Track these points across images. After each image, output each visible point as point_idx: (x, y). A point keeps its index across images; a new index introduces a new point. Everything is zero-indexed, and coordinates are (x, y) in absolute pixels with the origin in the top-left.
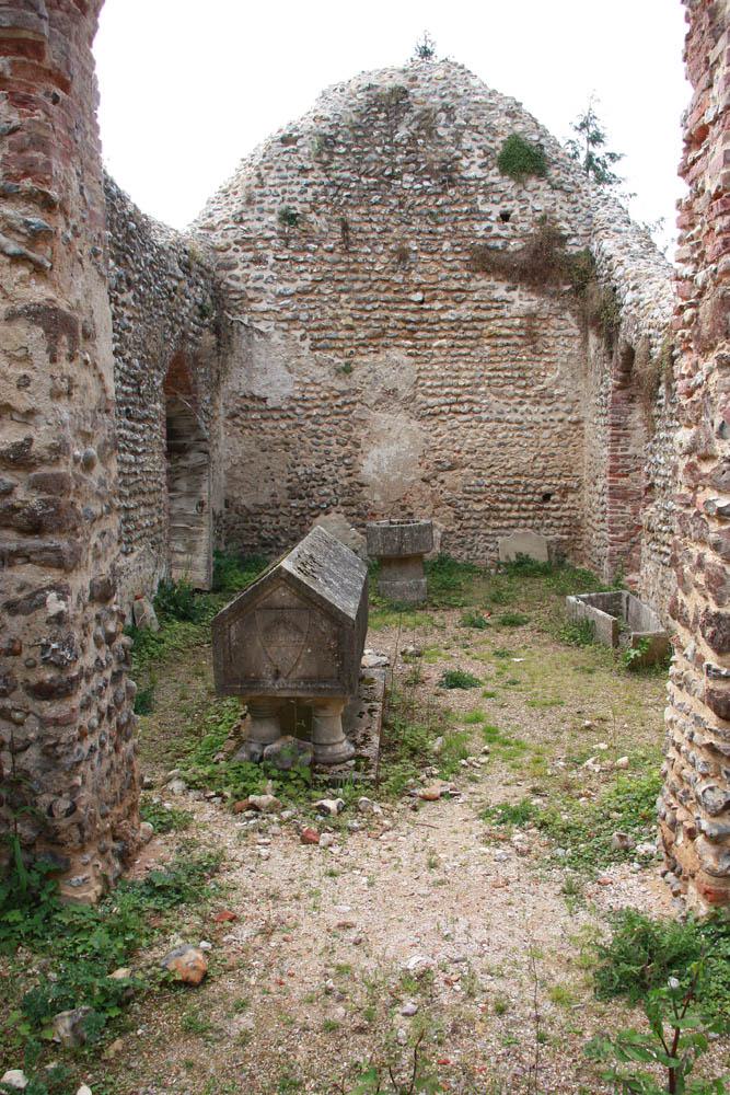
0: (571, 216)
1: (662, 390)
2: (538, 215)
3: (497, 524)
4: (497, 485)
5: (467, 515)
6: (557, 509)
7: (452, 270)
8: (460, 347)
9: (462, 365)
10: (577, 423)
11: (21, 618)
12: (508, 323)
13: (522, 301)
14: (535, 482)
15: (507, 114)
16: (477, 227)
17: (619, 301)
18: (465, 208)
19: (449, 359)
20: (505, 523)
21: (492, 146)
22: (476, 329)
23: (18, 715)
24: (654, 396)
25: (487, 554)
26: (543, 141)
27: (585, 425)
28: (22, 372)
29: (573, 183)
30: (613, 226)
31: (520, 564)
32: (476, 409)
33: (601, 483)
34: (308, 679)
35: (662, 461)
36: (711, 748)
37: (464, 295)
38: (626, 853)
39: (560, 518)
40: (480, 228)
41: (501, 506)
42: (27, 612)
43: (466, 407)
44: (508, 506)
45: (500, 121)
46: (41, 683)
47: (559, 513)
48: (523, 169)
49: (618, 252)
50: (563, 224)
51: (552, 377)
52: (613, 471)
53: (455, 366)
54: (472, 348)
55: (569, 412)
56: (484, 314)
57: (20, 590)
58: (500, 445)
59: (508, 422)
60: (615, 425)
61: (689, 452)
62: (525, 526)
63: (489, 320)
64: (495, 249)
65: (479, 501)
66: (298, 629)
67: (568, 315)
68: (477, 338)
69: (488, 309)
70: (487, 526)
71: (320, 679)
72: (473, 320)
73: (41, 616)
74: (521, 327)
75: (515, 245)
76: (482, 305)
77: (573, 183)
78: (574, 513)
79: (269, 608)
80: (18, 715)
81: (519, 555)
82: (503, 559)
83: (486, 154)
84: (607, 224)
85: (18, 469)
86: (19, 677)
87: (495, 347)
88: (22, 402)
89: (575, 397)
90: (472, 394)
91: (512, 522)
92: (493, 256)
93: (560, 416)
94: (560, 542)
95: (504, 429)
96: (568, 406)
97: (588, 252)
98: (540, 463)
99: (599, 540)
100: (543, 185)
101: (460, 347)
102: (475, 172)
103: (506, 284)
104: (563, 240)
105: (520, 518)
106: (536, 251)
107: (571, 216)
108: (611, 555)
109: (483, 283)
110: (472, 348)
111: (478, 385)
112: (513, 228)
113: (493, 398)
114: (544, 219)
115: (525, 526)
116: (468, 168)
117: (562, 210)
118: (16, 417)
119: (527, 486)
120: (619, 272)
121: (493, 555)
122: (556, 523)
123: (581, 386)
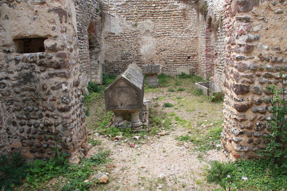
3: (176, 65)
4: (176, 54)
5: (168, 63)
8: (165, 18)
10: (197, 38)
11: (56, 91)
12: (178, 12)
14: (186, 53)
17: (207, 5)
19: (163, 22)
20: (178, 65)
22: (169, 13)
23: (56, 117)
25: (174, 73)
27: (199, 38)
28: (53, 26)
31: (182, 75)
32: (170, 35)
33: (203, 53)
34: (130, 106)
35: (219, 47)
37: (166, 5)
38: (214, 147)
39: (192, 63)
41: (177, 60)
43: (167, 34)
44: (179, 60)
47: (192, 62)
53: (164, 24)
54: (169, 19)
55: (194, 35)
56: (172, 10)
57: (55, 84)
58: (177, 44)
59: (178, 38)
62: (183, 65)
63: (173, 11)
65: (171, 59)
66: (127, 93)
67: (194, 9)
69: (173, 8)
70: (173, 65)
71: (133, 105)
72: (169, 11)
74: (181, 13)
76: (171, 7)
78: (196, 61)
80: (56, 117)
81: (182, 73)
82: (178, 74)
86: (56, 106)
88: (53, 34)
89: (196, 31)
91: (180, 64)
93: (192, 36)
94: (193, 69)
95: (178, 40)
98: (187, 49)
99: (203, 69)
101: (165, 18)
105: (182, 63)
108: (206, 72)
111: (170, 28)
113: (174, 32)
115: (183, 65)
119: (184, 55)
121: (175, 73)
122: (192, 64)
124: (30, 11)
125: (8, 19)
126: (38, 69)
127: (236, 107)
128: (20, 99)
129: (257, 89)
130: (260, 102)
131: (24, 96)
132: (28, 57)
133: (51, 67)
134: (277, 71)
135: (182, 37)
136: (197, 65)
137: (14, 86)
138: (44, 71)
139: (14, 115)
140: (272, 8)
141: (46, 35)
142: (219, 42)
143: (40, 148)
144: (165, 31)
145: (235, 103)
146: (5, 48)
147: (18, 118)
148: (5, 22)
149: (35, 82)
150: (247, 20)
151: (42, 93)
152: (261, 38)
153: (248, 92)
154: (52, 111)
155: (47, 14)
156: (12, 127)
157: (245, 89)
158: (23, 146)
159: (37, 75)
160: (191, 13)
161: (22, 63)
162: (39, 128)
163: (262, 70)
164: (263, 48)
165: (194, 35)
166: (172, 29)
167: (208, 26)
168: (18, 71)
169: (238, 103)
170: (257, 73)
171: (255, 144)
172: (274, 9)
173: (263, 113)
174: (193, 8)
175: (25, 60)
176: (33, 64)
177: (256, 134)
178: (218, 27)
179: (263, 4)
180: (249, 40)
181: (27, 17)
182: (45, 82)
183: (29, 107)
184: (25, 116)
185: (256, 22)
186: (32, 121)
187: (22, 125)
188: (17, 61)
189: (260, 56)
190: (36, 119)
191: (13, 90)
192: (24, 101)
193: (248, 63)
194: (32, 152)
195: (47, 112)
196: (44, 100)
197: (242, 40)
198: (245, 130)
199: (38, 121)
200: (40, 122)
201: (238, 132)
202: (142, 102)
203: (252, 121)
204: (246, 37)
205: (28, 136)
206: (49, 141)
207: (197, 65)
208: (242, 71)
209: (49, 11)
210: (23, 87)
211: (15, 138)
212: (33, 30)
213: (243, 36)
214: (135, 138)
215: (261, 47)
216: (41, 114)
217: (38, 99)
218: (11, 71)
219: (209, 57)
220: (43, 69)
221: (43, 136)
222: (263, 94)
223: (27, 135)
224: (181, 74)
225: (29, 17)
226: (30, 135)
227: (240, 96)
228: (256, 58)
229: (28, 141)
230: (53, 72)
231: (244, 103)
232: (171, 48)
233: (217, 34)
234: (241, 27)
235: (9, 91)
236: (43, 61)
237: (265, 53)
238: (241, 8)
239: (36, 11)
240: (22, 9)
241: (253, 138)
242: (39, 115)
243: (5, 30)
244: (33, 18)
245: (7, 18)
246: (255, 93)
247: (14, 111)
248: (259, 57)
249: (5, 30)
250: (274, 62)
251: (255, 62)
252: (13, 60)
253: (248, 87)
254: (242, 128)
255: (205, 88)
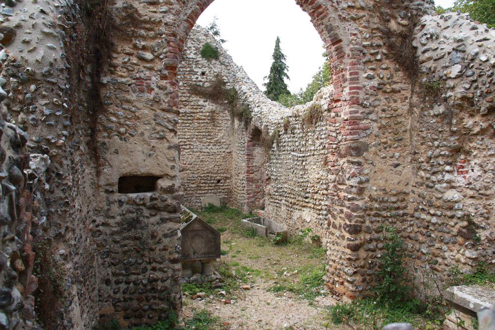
0: (228, 75)
1: (275, 145)
2: (216, 74)
3: (200, 192)
4: (200, 177)
5: (189, 189)
6: (223, 186)
7: (183, 93)
8: (186, 123)
9: (186, 130)
10: (230, 153)
11: (168, 239)
12: (204, 114)
13: (209, 106)
14: (214, 175)
15: (204, 35)
16: (193, 77)
17: (250, 110)
18: (188, 70)
19: (182, 128)
20: (203, 192)
21: (199, 46)
22: (192, 116)
23: (166, 269)
24: (270, 147)
25: (197, 204)
26: (217, 46)
27: (233, 153)
28: (172, 164)
29: (228, 63)
30: (244, 80)
31: (211, 208)
32: (192, 147)
33: (241, 177)
34: (205, 254)
35: (275, 170)
36: (349, 259)
37: (187, 103)
38: (318, 294)
39: (224, 189)
40: (194, 78)
41: (202, 185)
42: (170, 237)
43: (188, 147)
44: (204, 185)
45: (202, 37)
46: (174, 259)
47: (224, 187)
48: (210, 56)
49: (248, 91)
50: (225, 78)
51: (220, 135)
52: (248, 172)
53: (184, 130)
54: (190, 124)
55: (227, 149)
56: (195, 111)
57: (168, 230)
58: (201, 161)
59: (204, 152)
60: (248, 155)
61: (334, 182)
62: (211, 193)
63: (197, 113)
64: (199, 86)
65: (193, 183)
66: (203, 237)
67: (226, 112)
68: (192, 120)
69: (196, 109)
70: (196, 193)
71: (209, 253)
72: (191, 113)
73: (176, 238)
74: (209, 116)
75: (207, 85)
76: (195, 107)
77: (228, 63)
78: (229, 187)
79: (193, 231)
80: (166, 269)
81: (209, 204)
82: (203, 206)
83: (196, 49)
84: (242, 80)
85: (169, 193)
86: (167, 257)
87: (199, 123)
88: (172, 173)
89: (229, 143)
90: (190, 142)
91: (206, 191)
92: (199, 88)
93: (224, 150)
94: (224, 198)
95: (203, 155)
96: (226, 146)
97: (234, 89)
98: (216, 168)
99: (242, 197)
100: (217, 62)
101: (186, 123)
102: (192, 56)
103: (204, 99)
104: (225, 84)
105: (209, 189)
106: (215, 87)
107: (228, 75)
108: (248, 203)
109: (195, 99)
110: (190, 124)
111: (192, 138)
112: (206, 78)
113: (198, 143)
114: (218, 75)
115: (211, 193)
116: (189, 54)
117: (224, 73)
118: (169, 177)
119: (211, 177)
120: (251, 99)
121: (199, 204)
122: (223, 191)
123: (231, 139)
124: (145, 146)
125: (117, 153)
126: (146, 212)
127: (349, 247)
128: (120, 250)
129: (368, 227)
130: (371, 240)
131: (125, 246)
132: (136, 198)
133: (164, 211)
134: (384, 210)
135: (209, 151)
136: (230, 192)
137: (112, 234)
138: (154, 216)
139: (109, 270)
140: (379, 153)
141: (163, 173)
142: (274, 163)
143: (138, 312)
144: (185, 142)
145: (349, 242)
146: (108, 188)
147: (114, 274)
148: (114, 157)
149: (142, 228)
150: (359, 164)
151: (150, 241)
152: (371, 180)
153: (360, 231)
154: (161, 263)
155: (166, 151)
156: (104, 286)
157: (358, 228)
158: (117, 311)
159: (146, 220)
160: (223, 117)
161: (126, 206)
162: (141, 286)
163: (371, 209)
164: (373, 189)
165: (227, 149)
166: (194, 140)
167: (251, 138)
168: (121, 215)
169: (351, 243)
170: (367, 212)
171: (368, 283)
172: (380, 154)
173: (374, 251)
174: (225, 109)
175: (133, 202)
176: (141, 207)
177: (369, 272)
178: (273, 143)
179: (372, 149)
180: (361, 182)
181: (141, 153)
182: (155, 228)
183: (131, 259)
184: (124, 272)
185: (366, 166)
186: (133, 277)
187: (117, 282)
188: (121, 203)
189: (370, 197)
190: (138, 274)
191: (110, 239)
192: (125, 253)
193: (360, 203)
194: (126, 318)
195: (154, 264)
196: (152, 250)
197: (353, 182)
198: (359, 269)
199: (141, 277)
200: (143, 277)
201: (352, 271)
202: (221, 250)
203: (365, 259)
204: (357, 179)
205: (124, 298)
206: (152, 301)
207: (231, 192)
208: (354, 212)
209: (170, 148)
210: (124, 235)
211: (106, 301)
212: (145, 166)
213: (355, 178)
214: (221, 294)
215: (371, 189)
216: (145, 267)
217: (143, 249)
218: (113, 215)
219: (252, 182)
220: (154, 214)
221: (143, 296)
222: (373, 232)
223: (123, 295)
224: (207, 205)
225: (143, 152)
226: (127, 296)
227: (353, 235)
228: (367, 199)
229: (123, 303)
230: (167, 217)
231: (357, 242)
232: (193, 167)
233: (270, 152)
234: (353, 170)
235: (105, 240)
236: (156, 204)
237: (374, 194)
238: (353, 153)
239: (153, 147)
240: (136, 143)
241: (366, 276)
242: (143, 269)
243: (111, 166)
244: (148, 154)
245: (117, 152)
246: (366, 232)
247: (109, 266)
248: (369, 197)
249: (111, 166)
250: (381, 202)
251: (366, 202)
252: (116, 201)
253: (360, 227)
254: (355, 268)
255: (261, 227)
